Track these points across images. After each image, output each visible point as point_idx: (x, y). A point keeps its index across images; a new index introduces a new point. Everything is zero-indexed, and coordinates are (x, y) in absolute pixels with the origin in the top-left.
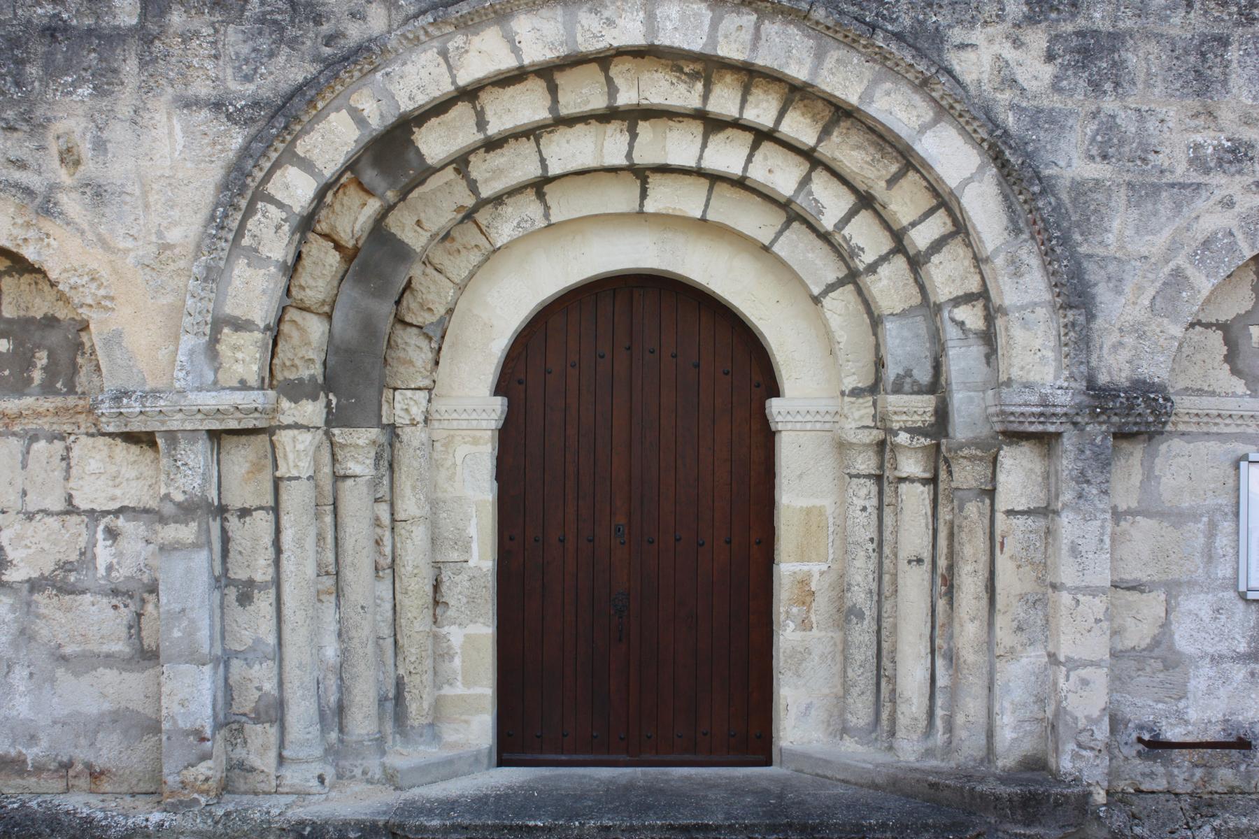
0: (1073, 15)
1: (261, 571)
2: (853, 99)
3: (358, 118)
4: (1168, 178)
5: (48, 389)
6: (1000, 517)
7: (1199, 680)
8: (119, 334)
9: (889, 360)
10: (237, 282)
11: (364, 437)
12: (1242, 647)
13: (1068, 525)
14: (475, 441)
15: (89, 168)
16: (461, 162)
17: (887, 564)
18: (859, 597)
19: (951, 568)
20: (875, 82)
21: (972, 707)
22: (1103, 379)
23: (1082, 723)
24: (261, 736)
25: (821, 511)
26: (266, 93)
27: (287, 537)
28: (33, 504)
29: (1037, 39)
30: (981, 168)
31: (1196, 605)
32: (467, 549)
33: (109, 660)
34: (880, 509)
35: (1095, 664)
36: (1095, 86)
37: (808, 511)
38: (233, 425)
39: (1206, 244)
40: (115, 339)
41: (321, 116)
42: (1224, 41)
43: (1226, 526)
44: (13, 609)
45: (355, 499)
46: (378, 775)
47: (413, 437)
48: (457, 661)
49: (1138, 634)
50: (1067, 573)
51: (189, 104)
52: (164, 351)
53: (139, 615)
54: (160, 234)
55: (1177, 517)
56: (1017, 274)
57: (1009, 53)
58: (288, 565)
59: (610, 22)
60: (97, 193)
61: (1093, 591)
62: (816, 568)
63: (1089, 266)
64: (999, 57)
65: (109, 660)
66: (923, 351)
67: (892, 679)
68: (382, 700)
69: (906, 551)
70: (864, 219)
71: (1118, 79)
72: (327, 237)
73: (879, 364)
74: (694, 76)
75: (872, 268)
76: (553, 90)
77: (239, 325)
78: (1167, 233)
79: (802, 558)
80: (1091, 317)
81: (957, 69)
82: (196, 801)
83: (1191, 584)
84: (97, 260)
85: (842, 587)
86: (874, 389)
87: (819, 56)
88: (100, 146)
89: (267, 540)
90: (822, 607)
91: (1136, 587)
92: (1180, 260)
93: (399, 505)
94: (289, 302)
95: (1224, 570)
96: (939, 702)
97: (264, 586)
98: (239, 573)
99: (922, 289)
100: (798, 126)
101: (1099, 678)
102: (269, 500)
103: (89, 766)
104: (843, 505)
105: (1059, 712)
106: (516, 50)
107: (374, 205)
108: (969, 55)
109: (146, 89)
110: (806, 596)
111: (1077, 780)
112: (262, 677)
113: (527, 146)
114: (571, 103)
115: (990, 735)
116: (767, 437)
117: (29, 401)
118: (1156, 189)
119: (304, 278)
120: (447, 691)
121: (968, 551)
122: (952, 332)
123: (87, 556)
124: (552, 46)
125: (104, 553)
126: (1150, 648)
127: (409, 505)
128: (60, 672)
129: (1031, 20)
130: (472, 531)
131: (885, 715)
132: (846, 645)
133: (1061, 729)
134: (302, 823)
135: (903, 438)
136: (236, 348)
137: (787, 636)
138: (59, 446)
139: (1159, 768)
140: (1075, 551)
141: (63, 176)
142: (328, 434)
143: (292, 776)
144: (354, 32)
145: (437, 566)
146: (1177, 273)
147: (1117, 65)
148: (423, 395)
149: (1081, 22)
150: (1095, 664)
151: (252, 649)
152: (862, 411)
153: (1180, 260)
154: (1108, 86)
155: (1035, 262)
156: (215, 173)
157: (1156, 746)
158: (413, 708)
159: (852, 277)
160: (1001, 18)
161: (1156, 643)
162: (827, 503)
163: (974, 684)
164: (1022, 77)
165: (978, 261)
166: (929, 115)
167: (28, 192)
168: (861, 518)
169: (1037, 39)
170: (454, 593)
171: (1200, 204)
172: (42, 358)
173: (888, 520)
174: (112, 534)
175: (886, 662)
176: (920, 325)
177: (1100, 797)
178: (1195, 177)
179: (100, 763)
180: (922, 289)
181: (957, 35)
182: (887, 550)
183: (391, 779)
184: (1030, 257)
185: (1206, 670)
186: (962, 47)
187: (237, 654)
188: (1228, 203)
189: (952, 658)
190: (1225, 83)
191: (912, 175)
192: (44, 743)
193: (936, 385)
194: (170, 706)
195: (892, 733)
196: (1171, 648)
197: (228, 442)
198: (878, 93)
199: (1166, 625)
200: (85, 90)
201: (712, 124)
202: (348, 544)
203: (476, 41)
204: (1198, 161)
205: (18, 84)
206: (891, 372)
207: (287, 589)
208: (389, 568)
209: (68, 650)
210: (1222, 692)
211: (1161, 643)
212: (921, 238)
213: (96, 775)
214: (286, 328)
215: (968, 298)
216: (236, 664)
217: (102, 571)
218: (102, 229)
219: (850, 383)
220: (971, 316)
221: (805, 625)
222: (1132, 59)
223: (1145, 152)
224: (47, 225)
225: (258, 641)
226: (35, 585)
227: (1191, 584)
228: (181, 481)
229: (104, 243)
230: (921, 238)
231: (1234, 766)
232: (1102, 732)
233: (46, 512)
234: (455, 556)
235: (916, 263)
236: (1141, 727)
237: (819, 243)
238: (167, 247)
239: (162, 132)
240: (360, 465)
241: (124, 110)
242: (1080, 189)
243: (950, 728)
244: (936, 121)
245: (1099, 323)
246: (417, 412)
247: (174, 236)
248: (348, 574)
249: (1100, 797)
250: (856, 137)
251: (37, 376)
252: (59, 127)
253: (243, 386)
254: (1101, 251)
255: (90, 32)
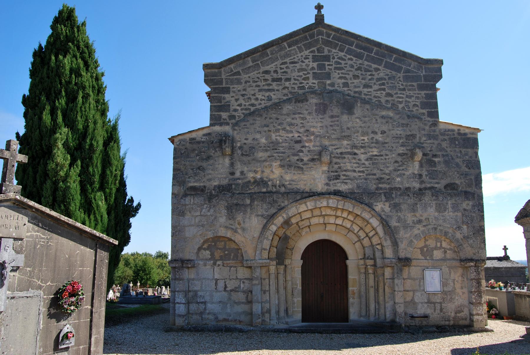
0: (393, 200)
1: (267, 289)
2: (359, 214)
3: (283, 217)
4: (409, 225)
5: (233, 260)
6: (385, 279)
7: (420, 306)
8: (246, 251)
9: (366, 254)
10: (265, 243)
11: (282, 267)
12: (426, 301)
13: (396, 281)
14: (298, 267)
15: (242, 225)
16: (297, 223)
17: (367, 288)
18: (363, 293)
19: (378, 288)
20: (362, 211)
21: (382, 311)
22: (400, 257)
23: (400, 313)
24: (267, 315)
25: (355, 279)
26: (270, 214)
27: (271, 283)
28: (231, 277)
29: (387, 204)
30: (380, 224)
31: (418, 294)
32: (297, 285)
33: (243, 303)
34: (366, 278)
35: (402, 303)
36: (397, 211)
37: (354, 279)
38: (264, 265)
39: (416, 235)
40: (246, 252)
41: (278, 217)
42: (417, 204)
43: (422, 281)
44: (228, 294)
45: (281, 277)
46: (285, 323)
47: (289, 267)
48: (296, 305)
49: (409, 299)
50: (396, 289)
51: (258, 216)
52: (417, 294)
53: (248, 296)
54: (253, 235)
55: (414, 279)
56: (386, 241)
57: (383, 207)
58: (271, 288)
59: (322, 203)
60: (244, 229)
61: (400, 291)
62: (355, 289)
63: (397, 239)
64: (382, 207)
65: (243, 303)
66: (372, 252)
67: (369, 307)
68: (285, 310)
69: (370, 285)
70: (361, 231)
71: (400, 210)
72: (277, 235)
73: (365, 255)
74: (334, 210)
75: (363, 239)
76: (312, 212)
77: (265, 249)
78: (409, 234)
79: (353, 287)
80: (398, 247)
81: (375, 209)
82: (258, 326)
83: (417, 290)
84: (243, 239)
85: (360, 292)
86: (364, 259)
87: (354, 207)
88: (244, 222)
89: (268, 283)
90: (356, 295)
91: (408, 291)
92: (412, 238)
93: (287, 278)
94: (271, 246)
95: (422, 288)
96: (377, 311)
97: (267, 291)
98: (264, 289)
99: (371, 242)
100: (351, 217)
101: (402, 305)
102: (268, 277)
103: (239, 320)
104: (360, 278)
105: (396, 311)
106: (307, 207)
107: (284, 230)
108: (377, 207)
109: (251, 214)
110: (354, 293)
111: (399, 323)
112: (267, 306)
113: (308, 220)
114: (315, 214)
115: (385, 316)
116: (346, 267)
117: (231, 261)
118: (407, 227)
119: (273, 242)
120: (294, 309)
121: (380, 285)
122: (376, 250)
123: (240, 286)
124: (313, 207)
125: (242, 286)
126: (411, 301)
127: (288, 278)
128: (235, 305)
129: (386, 201)
130: (298, 282)
131: (368, 314)
132: (361, 301)
133: (397, 314)
134: (275, 329)
135: (369, 267)
136: (264, 253)
137: (351, 300)
138: (235, 268)
139: (413, 321)
140: (397, 285)
141: (238, 226)
142: (277, 267)
143: (272, 322)
144: (283, 205)
145: (292, 288)
146: (411, 240)
147: (400, 208)
148: (290, 260)
149: (394, 201)
150: (402, 303)
151: (266, 301)
152: (362, 262)
153: (412, 238)
154: (399, 211)
155: (388, 239)
156: (262, 226)
157: (412, 317)
158: (289, 312)
159: (359, 240)
160: (382, 201)
161: (412, 300)
162: (357, 277)
163: (382, 307)
164: (385, 210)
165: (380, 238)
166: (371, 216)
167: (233, 229)
168: (362, 280)
169: (387, 204)
170: (295, 294)
171: (414, 230)
172: (233, 255)
173: (367, 280)
174: (243, 282)
175: (367, 304)
176: (371, 248)
177: (403, 325)
178: (413, 225)
179: (241, 320)
180: (371, 242)
181: (375, 204)
182: (367, 286)
183: (287, 323)
184: (388, 238)
185: (420, 305)
186: (376, 206)
187: (263, 302)
188: (419, 229)
189: (378, 303)
190: (417, 210)
191: (369, 225)
192: (232, 317)
193: (374, 259)
194: (254, 310)
195: (369, 316)
196: (414, 301)
197: (262, 268)
198: (363, 213)
199: (413, 297)
200: (242, 214)
201: (337, 217)
202: (280, 284)
203: (301, 206)
204: (413, 223)
205: (231, 213)
206: (367, 256)
207: (271, 291)
208: (285, 288)
209: (236, 301)
210: (423, 309)
211: (413, 300)
212: (371, 234)
213: (240, 322)
214: (271, 249)
215: (378, 244)
216: (263, 303)
217: (242, 288)
218: (244, 235)
219: (360, 257)
220: (379, 247)
221: (354, 298)
222: (402, 207)
223: (405, 221)
224: (235, 234)
225: (267, 300)
226: (231, 291)
227: (417, 290)
228: (256, 274)
229: (244, 237)
230: (371, 234)
231: (426, 321)
232: (403, 315)
233: (233, 279)
234: (295, 287)
235: (370, 238)
236: (410, 314)
237: (354, 235)
238: (254, 237)
239: (253, 220)
240: (282, 271)
241: (248, 217)
242: (395, 227)
243: (378, 314)
244: (372, 217)
245: (399, 248)
246: (289, 262)
247: (255, 236)
248: (280, 289)
249: (403, 325)
250: (360, 219)
251: (232, 257)
252: (238, 219)
253: (266, 259)
254: (399, 237)
255: (243, 205)
